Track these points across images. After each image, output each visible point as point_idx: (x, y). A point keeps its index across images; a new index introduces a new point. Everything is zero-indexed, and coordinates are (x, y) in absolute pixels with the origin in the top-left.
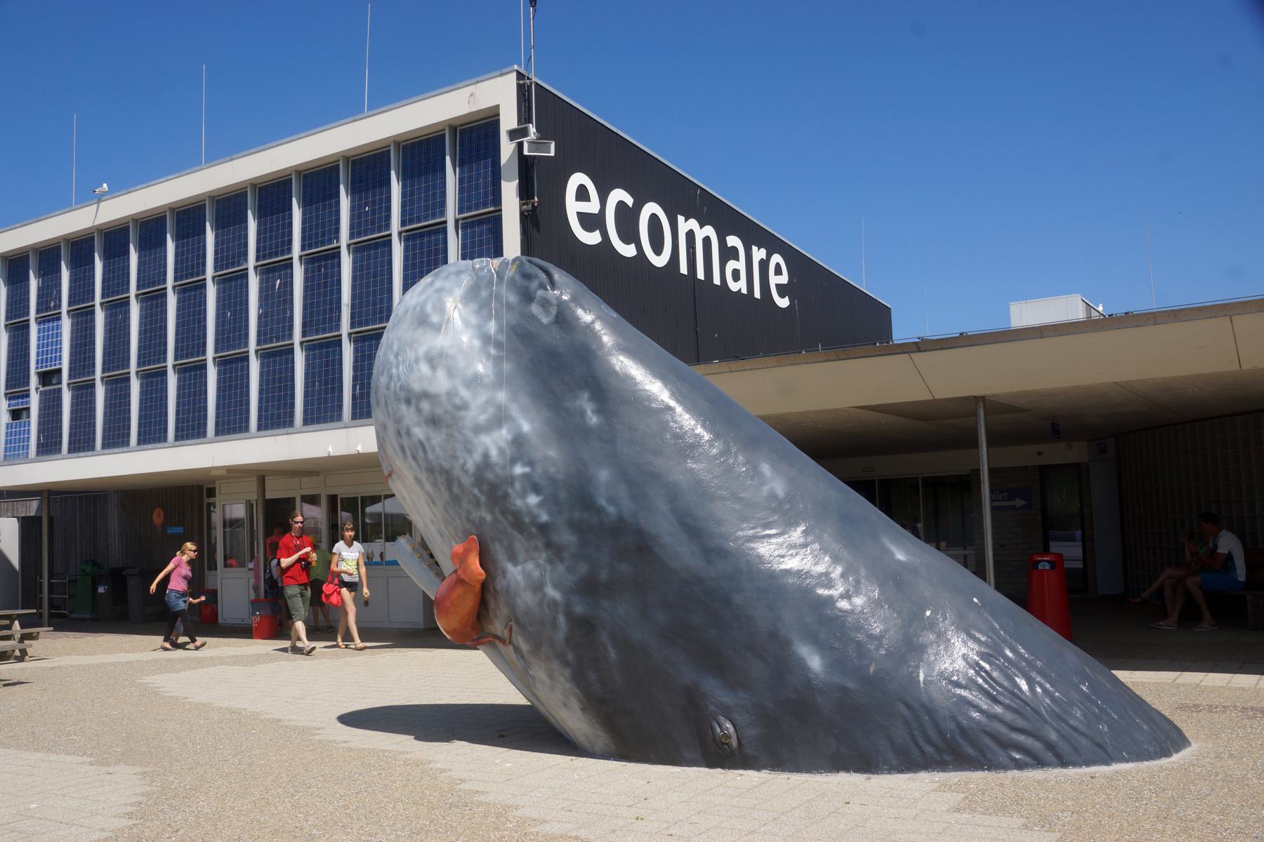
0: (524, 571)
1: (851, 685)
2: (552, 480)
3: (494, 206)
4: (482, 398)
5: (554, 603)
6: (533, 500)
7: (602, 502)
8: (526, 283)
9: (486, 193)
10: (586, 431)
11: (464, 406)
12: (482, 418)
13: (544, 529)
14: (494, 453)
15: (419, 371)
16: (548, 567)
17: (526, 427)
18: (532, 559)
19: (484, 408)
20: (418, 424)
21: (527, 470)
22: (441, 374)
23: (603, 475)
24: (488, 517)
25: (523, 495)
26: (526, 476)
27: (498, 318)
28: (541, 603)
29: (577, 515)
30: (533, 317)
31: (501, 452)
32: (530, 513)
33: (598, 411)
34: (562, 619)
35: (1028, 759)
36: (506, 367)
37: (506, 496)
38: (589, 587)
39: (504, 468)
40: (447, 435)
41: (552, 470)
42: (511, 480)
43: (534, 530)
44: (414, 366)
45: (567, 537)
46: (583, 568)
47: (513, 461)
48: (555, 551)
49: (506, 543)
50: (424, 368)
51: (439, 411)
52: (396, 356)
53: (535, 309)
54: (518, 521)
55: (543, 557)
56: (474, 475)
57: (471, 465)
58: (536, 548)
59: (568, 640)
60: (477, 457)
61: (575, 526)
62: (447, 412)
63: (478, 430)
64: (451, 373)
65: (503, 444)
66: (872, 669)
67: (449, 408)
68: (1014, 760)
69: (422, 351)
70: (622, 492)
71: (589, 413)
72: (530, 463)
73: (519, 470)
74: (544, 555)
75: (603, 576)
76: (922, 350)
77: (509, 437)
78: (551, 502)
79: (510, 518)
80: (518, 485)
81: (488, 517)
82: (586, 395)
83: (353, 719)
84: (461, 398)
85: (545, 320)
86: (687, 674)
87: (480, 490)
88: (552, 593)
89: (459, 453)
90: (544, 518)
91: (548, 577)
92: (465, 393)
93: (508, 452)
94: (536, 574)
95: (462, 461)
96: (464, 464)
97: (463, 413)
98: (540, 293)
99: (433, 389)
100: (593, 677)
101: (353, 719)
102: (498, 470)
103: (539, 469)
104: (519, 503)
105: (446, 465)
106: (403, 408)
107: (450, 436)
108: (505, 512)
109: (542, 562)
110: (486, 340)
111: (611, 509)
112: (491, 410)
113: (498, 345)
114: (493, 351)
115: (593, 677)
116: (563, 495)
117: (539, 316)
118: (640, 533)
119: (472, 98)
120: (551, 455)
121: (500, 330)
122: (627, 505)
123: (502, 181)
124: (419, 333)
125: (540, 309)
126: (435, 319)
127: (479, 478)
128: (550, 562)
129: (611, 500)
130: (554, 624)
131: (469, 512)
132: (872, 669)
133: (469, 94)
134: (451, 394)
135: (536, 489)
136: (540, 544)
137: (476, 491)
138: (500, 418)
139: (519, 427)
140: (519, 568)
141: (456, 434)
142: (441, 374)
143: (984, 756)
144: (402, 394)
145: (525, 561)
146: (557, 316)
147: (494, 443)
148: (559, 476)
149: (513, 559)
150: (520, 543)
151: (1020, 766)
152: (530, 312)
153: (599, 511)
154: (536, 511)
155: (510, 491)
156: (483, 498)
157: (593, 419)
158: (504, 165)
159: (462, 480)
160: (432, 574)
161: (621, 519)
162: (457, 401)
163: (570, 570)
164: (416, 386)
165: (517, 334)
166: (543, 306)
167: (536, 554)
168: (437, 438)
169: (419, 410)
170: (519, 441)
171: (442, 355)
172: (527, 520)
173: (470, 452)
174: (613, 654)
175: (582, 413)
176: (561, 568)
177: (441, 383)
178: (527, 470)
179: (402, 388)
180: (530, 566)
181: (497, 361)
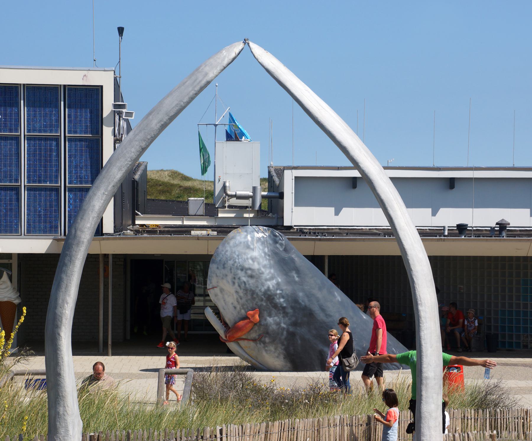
0: (273, 320)
1: (360, 349)
2: (287, 295)
3: (92, 134)
4: (268, 271)
5: (284, 328)
6: (282, 300)
7: (301, 301)
8: (275, 238)
9: (87, 126)
10: (295, 282)
11: (263, 273)
12: (268, 277)
13: (284, 308)
14: (271, 287)
15: (248, 262)
16: (282, 318)
17: (280, 280)
18: (277, 316)
19: (268, 274)
20: (245, 277)
21: (281, 292)
22: (256, 264)
23: (301, 294)
24: (264, 304)
25: (279, 299)
26: (280, 294)
27: (268, 248)
28: (279, 328)
29: (293, 304)
30: (277, 248)
31: (273, 286)
32: (280, 303)
33: (298, 277)
34: (285, 333)
35: (396, 368)
36: (272, 262)
37: (274, 299)
38: (295, 324)
39: (274, 291)
40: (256, 281)
41: (287, 292)
42: (276, 295)
43: (281, 308)
44: (246, 260)
45: (290, 311)
46: (293, 319)
47: (277, 289)
48: (285, 314)
49: (269, 311)
50: (250, 261)
51: (254, 274)
52: (238, 256)
53: (278, 245)
54: (276, 306)
55: (281, 316)
56: (263, 292)
57: (263, 290)
58: (280, 313)
59: (285, 339)
60: (266, 287)
61: (292, 308)
62: (257, 274)
63: (266, 280)
64: (259, 264)
65: (274, 285)
66: (364, 345)
67: (258, 273)
68: (393, 368)
69: (249, 256)
70: (306, 300)
71: (295, 277)
72: (282, 290)
73: (278, 292)
74: (282, 315)
75: (299, 321)
76: (117, 145)
77: (276, 283)
78: (287, 301)
79: (273, 305)
80: (278, 296)
81: (264, 304)
82: (294, 272)
83: (141, 370)
84: (262, 271)
85: (281, 249)
86: (321, 347)
87: (264, 297)
88: (283, 325)
89: (259, 286)
90: (285, 305)
91: (282, 321)
92: (263, 270)
93: (275, 287)
94: (278, 320)
95: (260, 288)
96: (261, 289)
97: (262, 275)
98: (280, 241)
99: (253, 267)
100: (291, 348)
101: (141, 370)
102: (272, 292)
103: (284, 292)
104: (277, 301)
105: (253, 289)
106: (239, 272)
107: (257, 281)
108: (271, 303)
109: (280, 317)
110: (265, 253)
111: (303, 303)
112: (270, 275)
113: (269, 256)
114: (268, 257)
115: (291, 348)
116: (290, 299)
117: (279, 248)
118: (310, 310)
119: (85, 78)
120: (287, 289)
121: (269, 251)
122: (307, 303)
123: (103, 126)
124: (247, 251)
125: (280, 246)
126: (252, 247)
127: (265, 293)
128: (283, 317)
129: (303, 301)
130: (282, 334)
131: (257, 302)
132: (364, 345)
133: (83, 75)
134: (259, 270)
135: (283, 297)
136: (281, 312)
137: (263, 297)
138: (272, 278)
139: (278, 280)
140: (272, 318)
141: (259, 281)
142: (256, 264)
143: (388, 367)
144: (240, 267)
145: (274, 317)
146: (285, 248)
147: (271, 284)
148: (289, 294)
149: (270, 316)
150: (274, 311)
151: (395, 369)
152: (277, 246)
153: (300, 304)
154: (282, 303)
155: (275, 297)
156: (265, 299)
157: (297, 279)
158: (104, 117)
159: (259, 293)
160: (218, 319)
161: (306, 306)
162: (261, 272)
163: (289, 319)
164: (247, 266)
165: (274, 253)
166: (280, 245)
167: (279, 315)
168: (252, 281)
169: (246, 273)
170: (278, 284)
171: (256, 258)
172: (279, 306)
173: (263, 286)
174: (299, 342)
175: (294, 277)
176: (287, 319)
177: (256, 266)
178: (281, 292)
179: (240, 266)
180: (276, 318)
181: (269, 260)
